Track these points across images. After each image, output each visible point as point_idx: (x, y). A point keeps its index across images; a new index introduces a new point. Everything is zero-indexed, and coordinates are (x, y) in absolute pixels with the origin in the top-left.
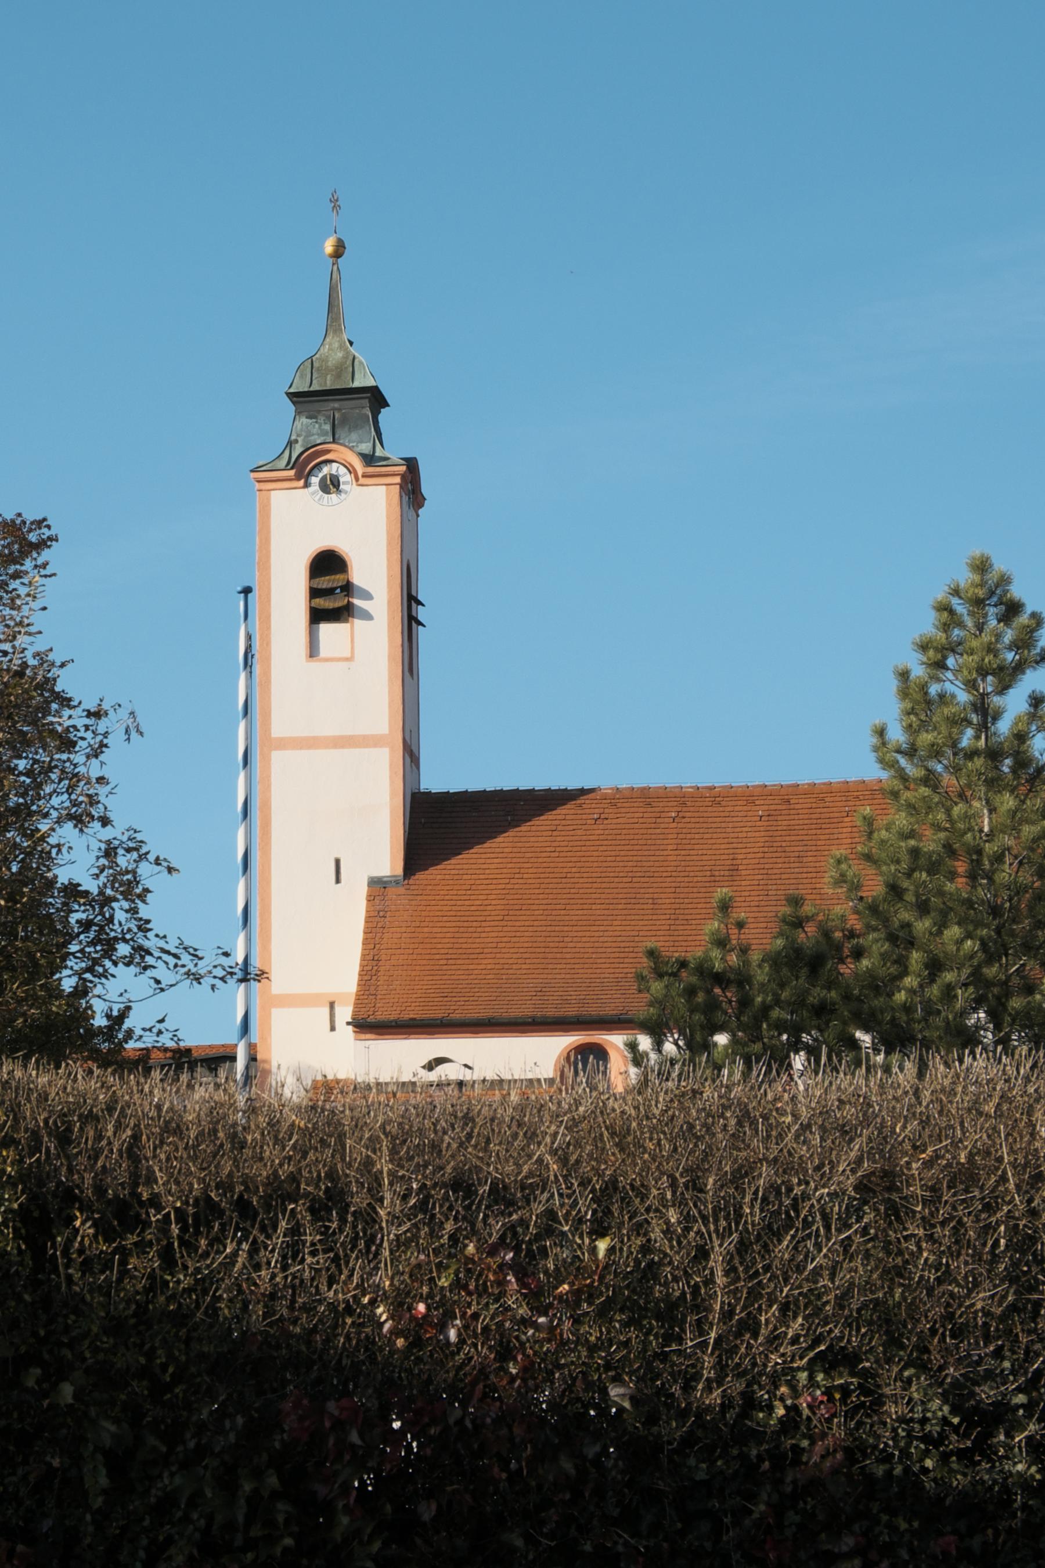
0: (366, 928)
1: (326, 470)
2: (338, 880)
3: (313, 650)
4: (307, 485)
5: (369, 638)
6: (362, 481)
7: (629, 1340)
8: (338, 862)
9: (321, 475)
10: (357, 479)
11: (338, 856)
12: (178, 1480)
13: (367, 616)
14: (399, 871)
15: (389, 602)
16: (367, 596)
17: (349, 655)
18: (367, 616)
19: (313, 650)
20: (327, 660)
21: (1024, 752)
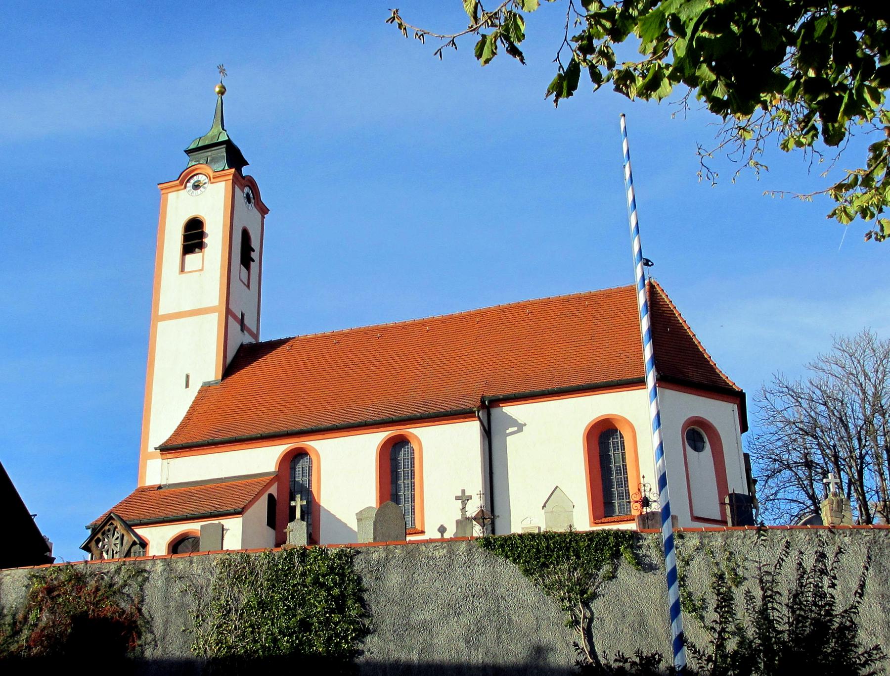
6: (212, 180)
8: (188, 377)
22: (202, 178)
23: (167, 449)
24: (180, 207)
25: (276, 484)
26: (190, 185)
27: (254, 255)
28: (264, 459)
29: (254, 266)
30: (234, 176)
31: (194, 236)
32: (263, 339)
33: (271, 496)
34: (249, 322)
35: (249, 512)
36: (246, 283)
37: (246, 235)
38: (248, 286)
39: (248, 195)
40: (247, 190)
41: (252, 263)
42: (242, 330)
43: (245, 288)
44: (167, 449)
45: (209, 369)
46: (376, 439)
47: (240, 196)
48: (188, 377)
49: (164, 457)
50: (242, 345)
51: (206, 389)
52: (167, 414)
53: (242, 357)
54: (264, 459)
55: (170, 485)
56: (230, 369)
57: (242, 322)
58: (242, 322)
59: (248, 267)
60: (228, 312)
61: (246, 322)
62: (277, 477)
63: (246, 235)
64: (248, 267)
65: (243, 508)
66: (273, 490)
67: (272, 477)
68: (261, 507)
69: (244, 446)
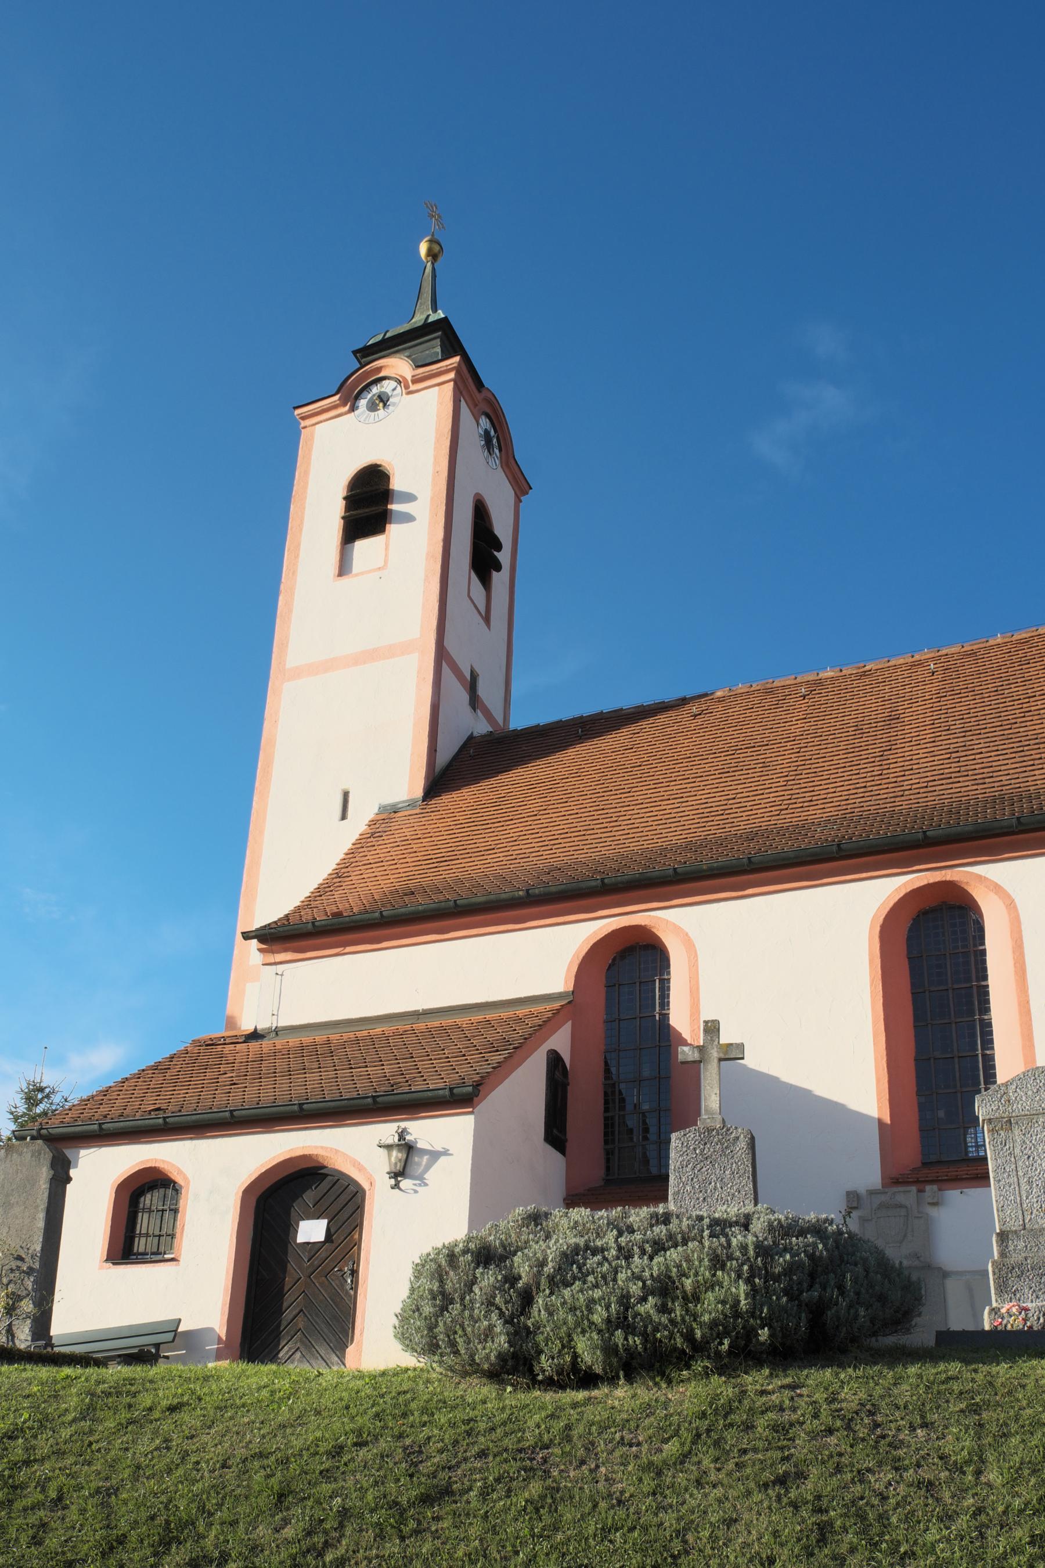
0: (992, 1035)
1: (375, 390)
2: (344, 817)
3: (344, 568)
4: (353, 409)
5: (412, 549)
6: (413, 387)
7: (851, 1543)
8: (346, 795)
9: (369, 396)
10: (407, 387)
11: (345, 787)
12: (410, 1526)
13: (408, 518)
14: (419, 793)
15: (432, 499)
16: (410, 498)
17: (382, 564)
18: (408, 518)
19: (344, 568)
20: (362, 573)
21: (639, 1374)
22: (387, 386)
23: (285, 937)
24: (334, 448)
25: (568, 1026)
26: (363, 403)
27: (503, 557)
28: (538, 960)
29: (499, 580)
30: (458, 370)
31: (369, 504)
32: (519, 722)
33: (555, 1060)
34: (490, 692)
35: (497, 1098)
36: (482, 608)
37: (481, 513)
38: (487, 619)
39: (487, 433)
40: (484, 422)
41: (494, 574)
42: (474, 676)
43: (482, 621)
44: (285, 937)
45: (398, 772)
46: (859, 905)
47: (473, 429)
48: (346, 795)
49: (271, 958)
50: (471, 738)
51: (389, 814)
52: (291, 861)
53: (467, 760)
54: (538, 960)
55: (277, 1031)
56: (440, 781)
57: (472, 686)
58: (472, 686)
59: (485, 580)
60: (442, 655)
61: (481, 691)
62: (568, 1007)
63: (481, 513)
64: (485, 580)
65: (477, 1086)
66: (561, 1041)
67: (557, 1005)
68: (525, 1089)
69: (124, 1222)
